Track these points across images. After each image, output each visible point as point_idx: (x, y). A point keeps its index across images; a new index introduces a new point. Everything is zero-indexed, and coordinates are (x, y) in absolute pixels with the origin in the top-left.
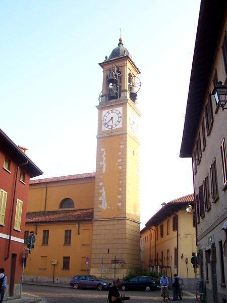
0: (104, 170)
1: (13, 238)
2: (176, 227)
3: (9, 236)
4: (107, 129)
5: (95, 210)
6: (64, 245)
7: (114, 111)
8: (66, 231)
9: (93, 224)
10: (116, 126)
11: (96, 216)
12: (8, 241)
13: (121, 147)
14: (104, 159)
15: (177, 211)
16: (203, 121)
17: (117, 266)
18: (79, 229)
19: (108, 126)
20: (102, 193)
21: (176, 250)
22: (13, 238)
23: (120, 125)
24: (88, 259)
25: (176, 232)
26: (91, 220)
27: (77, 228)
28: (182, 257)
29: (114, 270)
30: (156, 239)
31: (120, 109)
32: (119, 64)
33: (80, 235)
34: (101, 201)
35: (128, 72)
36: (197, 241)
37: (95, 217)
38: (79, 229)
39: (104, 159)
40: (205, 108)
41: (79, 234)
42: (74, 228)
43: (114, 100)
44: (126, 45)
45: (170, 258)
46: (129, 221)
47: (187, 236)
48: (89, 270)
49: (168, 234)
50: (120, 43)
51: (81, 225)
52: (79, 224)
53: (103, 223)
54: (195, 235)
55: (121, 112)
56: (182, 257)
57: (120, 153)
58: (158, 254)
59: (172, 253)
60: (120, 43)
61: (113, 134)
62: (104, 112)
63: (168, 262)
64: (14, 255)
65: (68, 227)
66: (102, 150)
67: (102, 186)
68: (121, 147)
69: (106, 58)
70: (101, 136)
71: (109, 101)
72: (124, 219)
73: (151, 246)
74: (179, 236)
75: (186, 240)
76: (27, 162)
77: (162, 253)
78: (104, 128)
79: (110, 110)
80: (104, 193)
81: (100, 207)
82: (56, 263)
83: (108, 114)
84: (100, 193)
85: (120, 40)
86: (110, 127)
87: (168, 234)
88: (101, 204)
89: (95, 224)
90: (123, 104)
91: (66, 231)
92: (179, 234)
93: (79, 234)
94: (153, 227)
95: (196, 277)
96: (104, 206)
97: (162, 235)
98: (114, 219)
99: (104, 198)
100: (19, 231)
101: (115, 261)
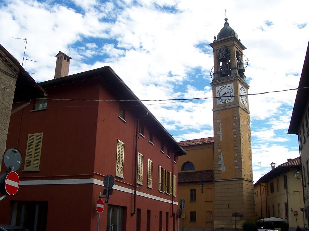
0: (221, 138)
1: (138, 193)
2: (286, 186)
3: (172, 201)
4: (221, 103)
5: (215, 172)
6: (191, 202)
7: (227, 87)
8: (191, 190)
9: (214, 184)
10: (229, 100)
11: (217, 177)
12: (172, 204)
13: (235, 118)
14: (221, 129)
15: (286, 172)
16: (307, 116)
17: (237, 218)
18: (202, 188)
19: (222, 100)
20: (220, 158)
21: (286, 205)
22: (138, 193)
23: (232, 100)
24: (211, 213)
25: (286, 189)
26: (213, 181)
27: (201, 187)
28: (292, 210)
29: (234, 222)
30: (267, 194)
31: (232, 85)
32: (227, 44)
33: (203, 193)
34: (220, 165)
35: (236, 50)
36: (304, 200)
37: (216, 178)
38: (202, 188)
39: (221, 129)
40: (307, 109)
41: (203, 193)
42: (198, 188)
43: (225, 77)
44: (231, 25)
45: (281, 211)
46: (245, 181)
47: (296, 193)
48: (213, 222)
49: (278, 191)
50: (226, 24)
51: (203, 185)
52: (202, 185)
53: (223, 183)
54: (303, 192)
55: (233, 88)
56: (292, 210)
57: (234, 124)
58: (269, 208)
59: (283, 207)
60: (226, 24)
61: (226, 107)
62: (218, 88)
63: (279, 214)
64: (139, 210)
65: (193, 187)
66: (218, 121)
67: (220, 152)
68: (235, 118)
69: (215, 38)
70: (216, 109)
71: (221, 79)
72: (241, 179)
73: (262, 201)
74: (288, 193)
75: (294, 196)
76: (179, 149)
77: (273, 206)
78: (219, 102)
79: (222, 86)
80: (222, 158)
81: (220, 170)
82: (184, 217)
83: (223, 90)
84: (219, 158)
85: (226, 20)
86: (224, 101)
87: (278, 191)
88: (220, 167)
89: (216, 184)
90: (233, 81)
91: (191, 190)
92: (288, 191)
93: (203, 193)
94: (264, 184)
95: (304, 226)
96: (223, 169)
97: (272, 191)
98: (232, 180)
99: (223, 162)
100: (142, 185)
101: (235, 215)
